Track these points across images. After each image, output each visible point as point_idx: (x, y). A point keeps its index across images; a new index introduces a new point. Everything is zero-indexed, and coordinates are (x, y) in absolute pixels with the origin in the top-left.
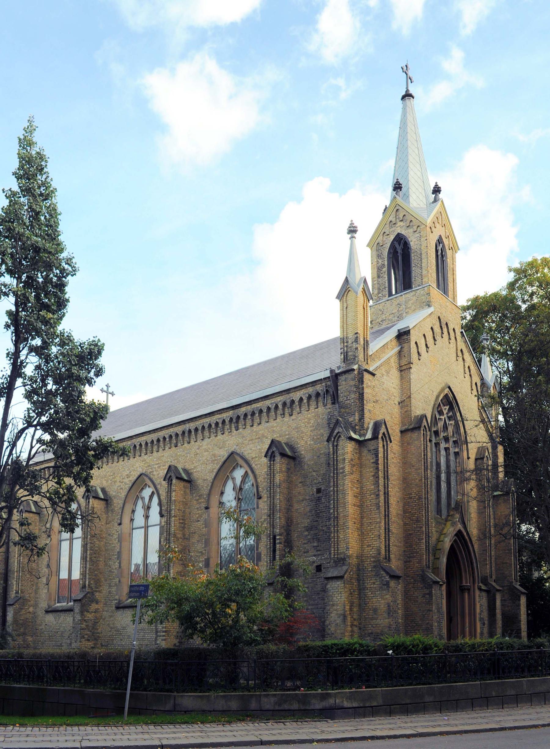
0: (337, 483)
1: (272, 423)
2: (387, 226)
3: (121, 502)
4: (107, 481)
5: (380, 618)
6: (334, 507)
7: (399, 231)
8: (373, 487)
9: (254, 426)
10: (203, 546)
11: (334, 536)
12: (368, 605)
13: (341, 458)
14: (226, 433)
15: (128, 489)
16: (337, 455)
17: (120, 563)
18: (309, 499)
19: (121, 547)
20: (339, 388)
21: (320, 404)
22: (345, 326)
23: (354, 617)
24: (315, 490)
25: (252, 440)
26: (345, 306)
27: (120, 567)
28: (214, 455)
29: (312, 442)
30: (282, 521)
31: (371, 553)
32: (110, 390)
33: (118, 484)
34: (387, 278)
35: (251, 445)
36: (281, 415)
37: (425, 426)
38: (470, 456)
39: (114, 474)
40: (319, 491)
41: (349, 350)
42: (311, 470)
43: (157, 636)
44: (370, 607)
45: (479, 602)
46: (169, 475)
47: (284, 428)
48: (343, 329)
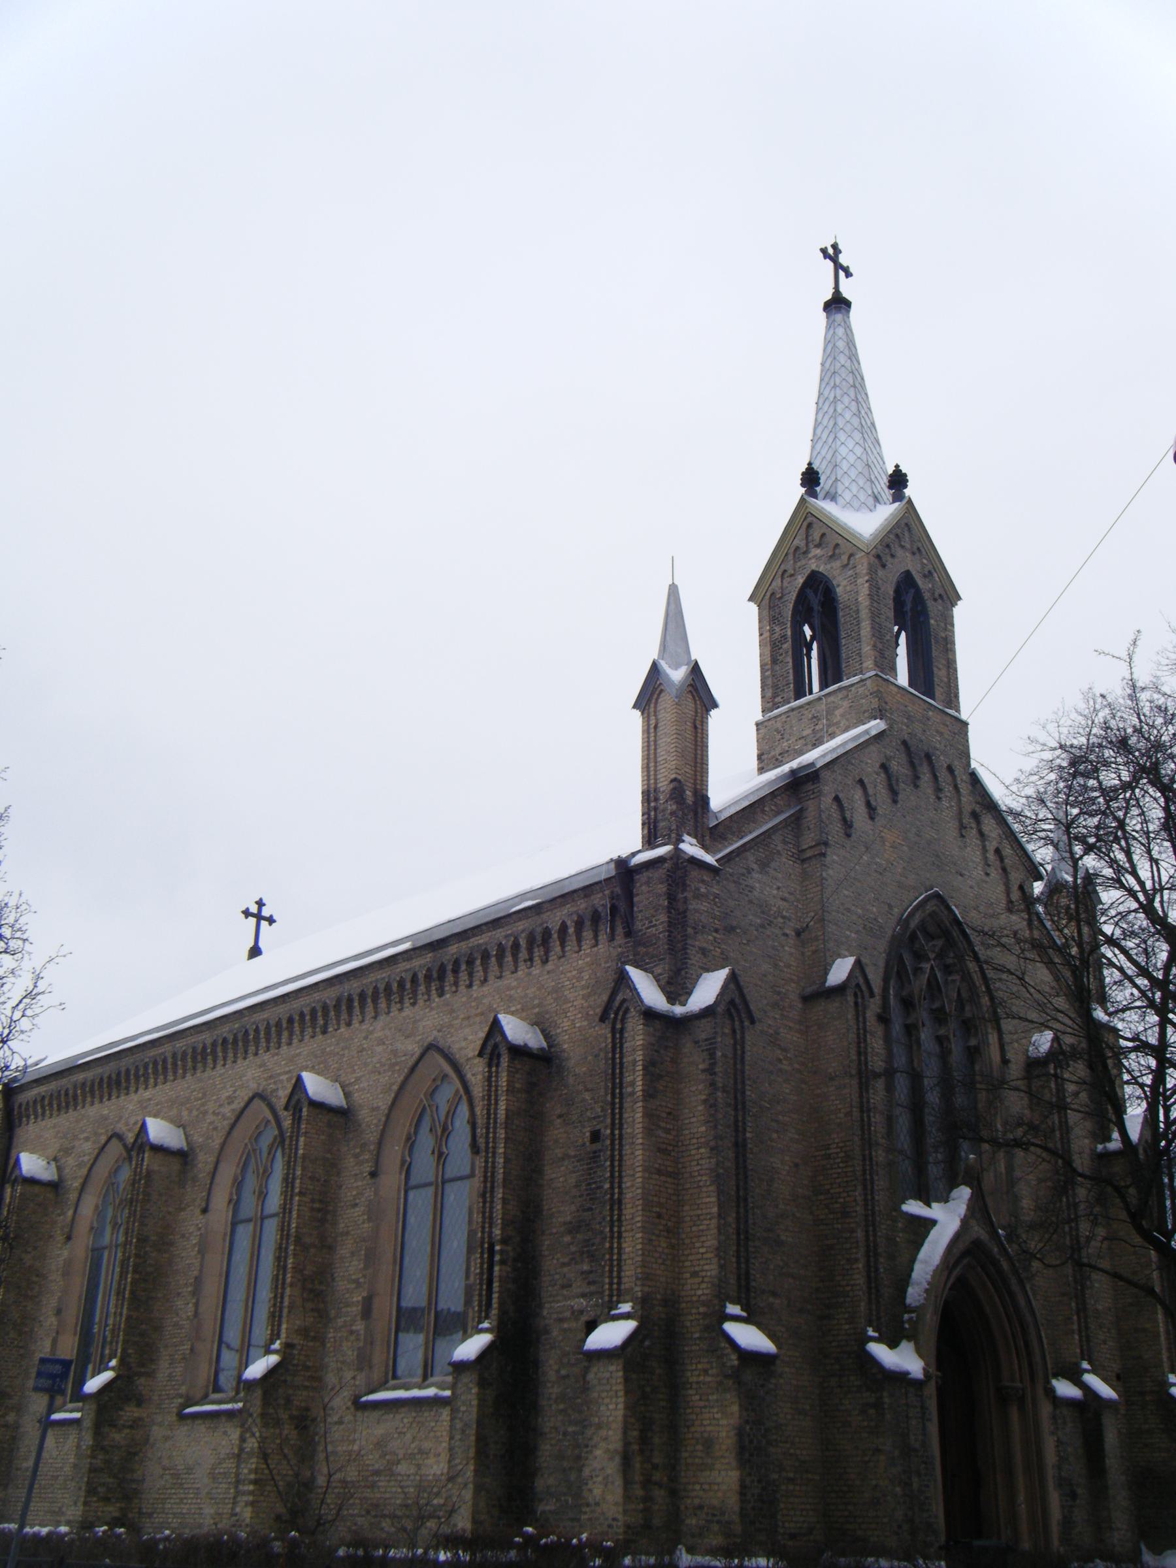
0: (621, 1118)
1: (510, 980)
2: (791, 557)
3: (212, 1159)
4: (190, 1111)
5: (718, 1466)
6: (612, 1176)
7: (814, 567)
8: (703, 1129)
9: (475, 988)
10: (362, 1266)
11: (611, 1248)
12: (693, 1429)
13: (630, 1058)
14: (421, 1002)
15: (227, 1128)
16: (621, 1052)
17: (197, 1305)
18: (575, 1156)
19: (202, 1266)
20: (636, 899)
21: (603, 937)
22: (652, 764)
23: (656, 1460)
24: (588, 1134)
25: (469, 1018)
26: (653, 722)
27: (196, 1314)
28: (395, 1053)
29: (585, 1023)
30: (510, 1207)
31: (699, 1292)
32: (266, 912)
33: (210, 1118)
34: (790, 665)
35: (467, 1031)
36: (525, 961)
37: (858, 985)
38: (1009, 1056)
39: (204, 1094)
40: (596, 1136)
41: (660, 817)
42: (581, 1087)
43: (238, 1493)
44: (697, 1435)
45: (1052, 1433)
46: (296, 1097)
47: (531, 991)
48: (648, 771)
